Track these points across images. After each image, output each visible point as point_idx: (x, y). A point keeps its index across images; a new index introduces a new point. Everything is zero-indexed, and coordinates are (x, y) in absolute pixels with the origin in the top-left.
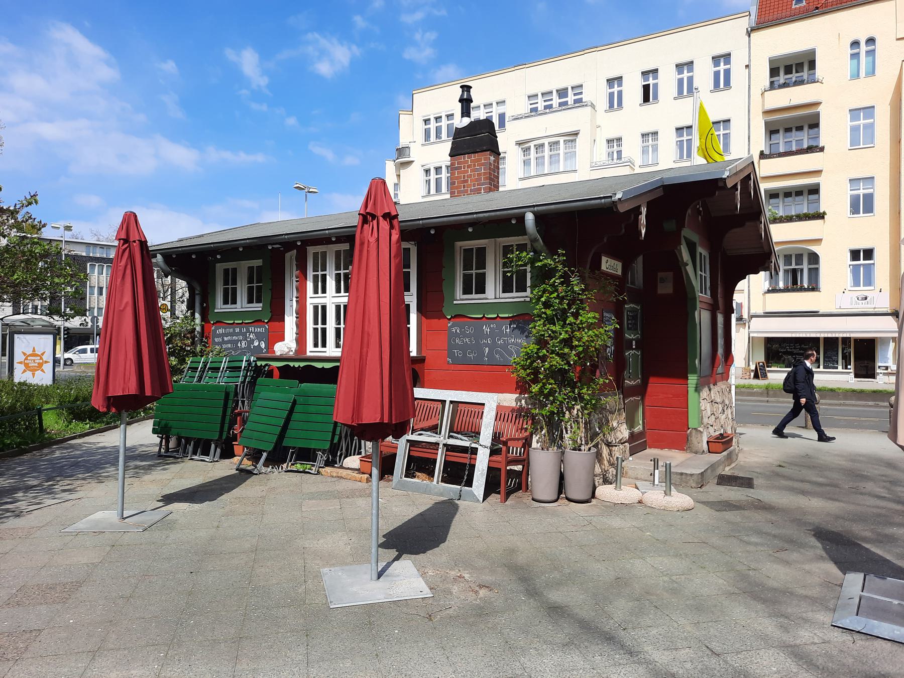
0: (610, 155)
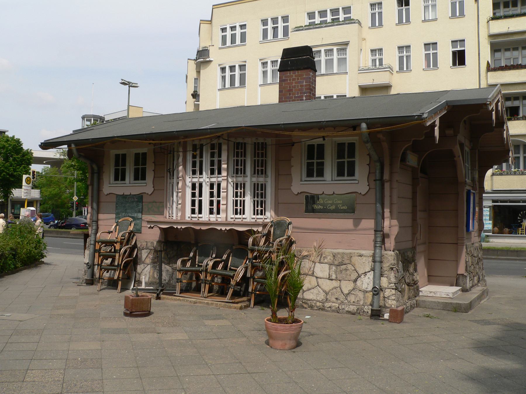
0: (374, 61)
